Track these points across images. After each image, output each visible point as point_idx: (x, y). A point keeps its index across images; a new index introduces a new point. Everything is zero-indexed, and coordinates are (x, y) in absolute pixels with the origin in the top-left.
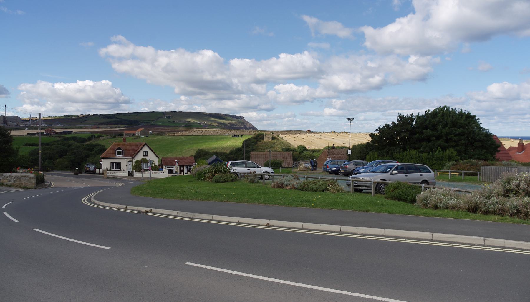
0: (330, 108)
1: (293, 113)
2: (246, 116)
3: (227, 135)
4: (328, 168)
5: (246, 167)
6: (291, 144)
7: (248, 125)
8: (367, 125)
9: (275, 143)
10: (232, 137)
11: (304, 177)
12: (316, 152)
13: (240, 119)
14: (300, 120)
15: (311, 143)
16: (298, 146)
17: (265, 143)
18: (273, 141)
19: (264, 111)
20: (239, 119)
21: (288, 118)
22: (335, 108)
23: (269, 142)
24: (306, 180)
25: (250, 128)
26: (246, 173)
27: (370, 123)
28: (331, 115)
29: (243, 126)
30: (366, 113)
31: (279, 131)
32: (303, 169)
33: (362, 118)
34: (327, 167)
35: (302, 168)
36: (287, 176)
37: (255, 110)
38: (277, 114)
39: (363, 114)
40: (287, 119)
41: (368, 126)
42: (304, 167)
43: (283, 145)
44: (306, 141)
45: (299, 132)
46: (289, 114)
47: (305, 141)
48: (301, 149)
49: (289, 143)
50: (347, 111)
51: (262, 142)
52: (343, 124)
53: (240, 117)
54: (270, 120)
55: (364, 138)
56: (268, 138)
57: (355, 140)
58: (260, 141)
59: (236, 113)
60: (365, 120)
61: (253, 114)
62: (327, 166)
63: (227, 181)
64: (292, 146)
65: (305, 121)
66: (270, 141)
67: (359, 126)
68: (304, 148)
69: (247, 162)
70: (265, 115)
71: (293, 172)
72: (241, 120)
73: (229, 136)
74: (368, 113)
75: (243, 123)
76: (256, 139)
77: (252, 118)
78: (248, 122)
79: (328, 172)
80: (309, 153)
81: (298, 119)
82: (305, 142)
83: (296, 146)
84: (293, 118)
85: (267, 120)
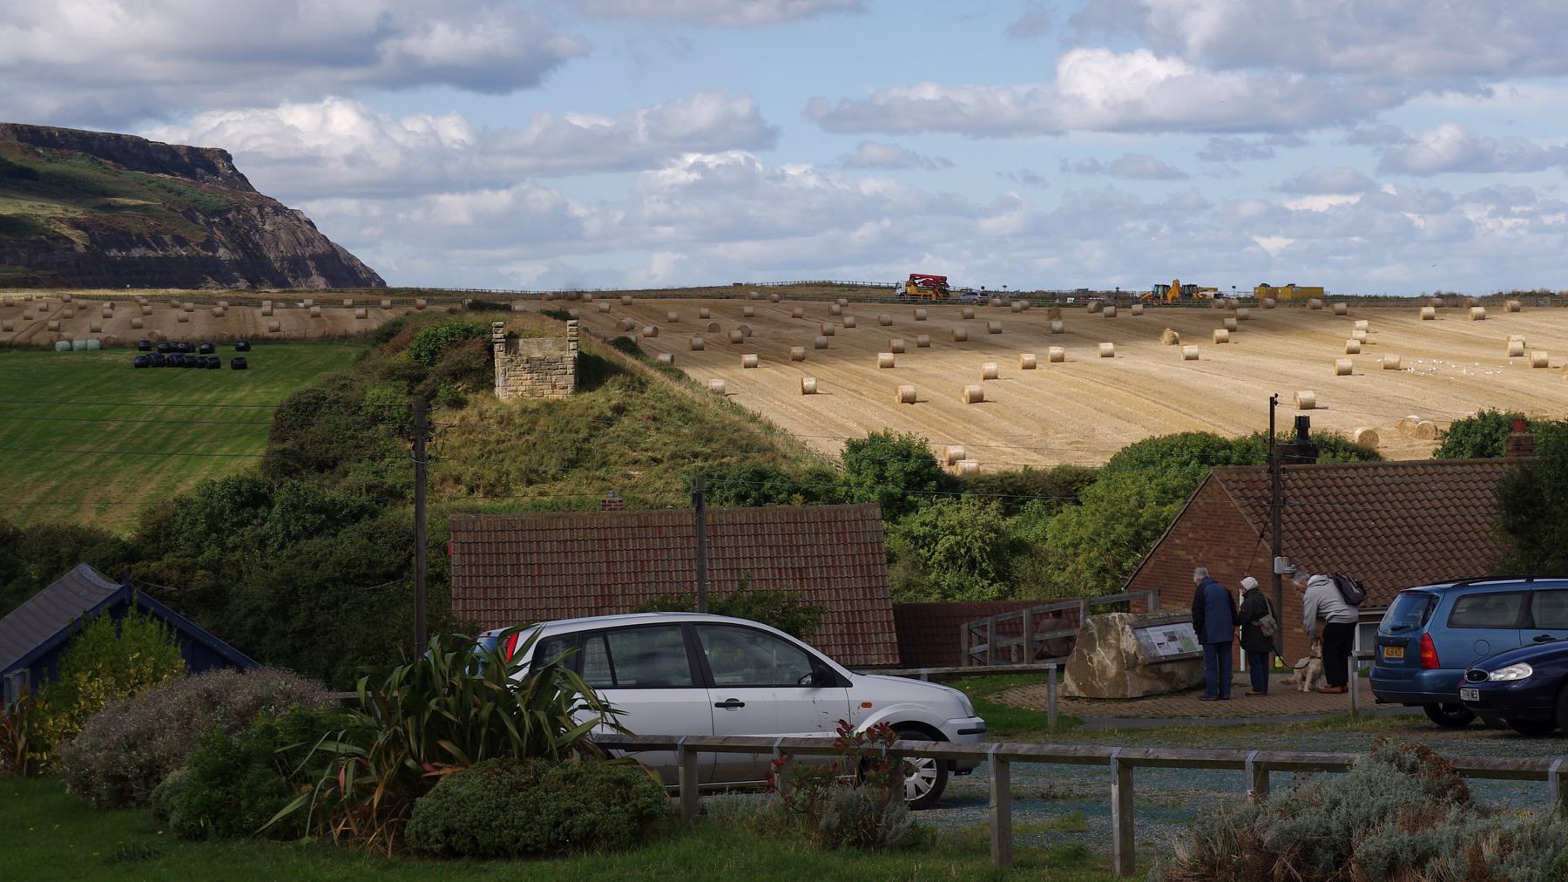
0: (1116, 51)
1: (743, 107)
2: (252, 145)
3: (84, 350)
4: (1426, 666)
5: (702, 679)
6: (770, 428)
7: (283, 235)
8: (1493, 215)
9: (609, 422)
10: (142, 364)
11: (1543, 776)
12: (1036, 504)
13: (192, 174)
14: (812, 181)
15: (976, 409)
16: (855, 447)
17: (505, 421)
18: (586, 397)
19: (444, 92)
20: (182, 182)
21: (691, 158)
22: (1168, 43)
23: (550, 407)
24: (1262, 788)
25: (298, 267)
26: (769, 750)
27: (1526, 196)
28: (1132, 121)
29: (222, 253)
30: (1489, 93)
31: (616, 295)
32: (1119, 681)
33: (1441, 140)
34: (1419, 652)
35: (1112, 670)
36: (1341, 768)
37: (346, 74)
38: (578, 121)
39: (1454, 100)
40: (680, 171)
41: (1508, 223)
42: (1129, 663)
43: (698, 436)
44: (923, 392)
45: (835, 299)
46: (704, 112)
47: (908, 389)
48: (881, 478)
49: (754, 419)
50: (1296, 78)
51: (470, 413)
52: (1249, 208)
53: (192, 151)
54: (508, 186)
55: (1501, 345)
56: (534, 366)
57: (1413, 364)
58: (458, 403)
59: (150, 112)
60: (1473, 159)
61: (326, 120)
62: (1424, 644)
63: (586, 841)
64: (780, 443)
65: (871, 184)
66: (558, 395)
67: (1419, 222)
68: (912, 465)
69: (703, 636)
70: (453, 130)
71: (1051, 721)
72: (208, 192)
73: (106, 357)
74: (1501, 90)
75: (217, 213)
76: (415, 379)
77: (312, 159)
78: (279, 209)
79: (1420, 710)
80: (965, 514)
81: (792, 171)
82: (909, 400)
83: (830, 449)
84: (738, 156)
85: (471, 184)
